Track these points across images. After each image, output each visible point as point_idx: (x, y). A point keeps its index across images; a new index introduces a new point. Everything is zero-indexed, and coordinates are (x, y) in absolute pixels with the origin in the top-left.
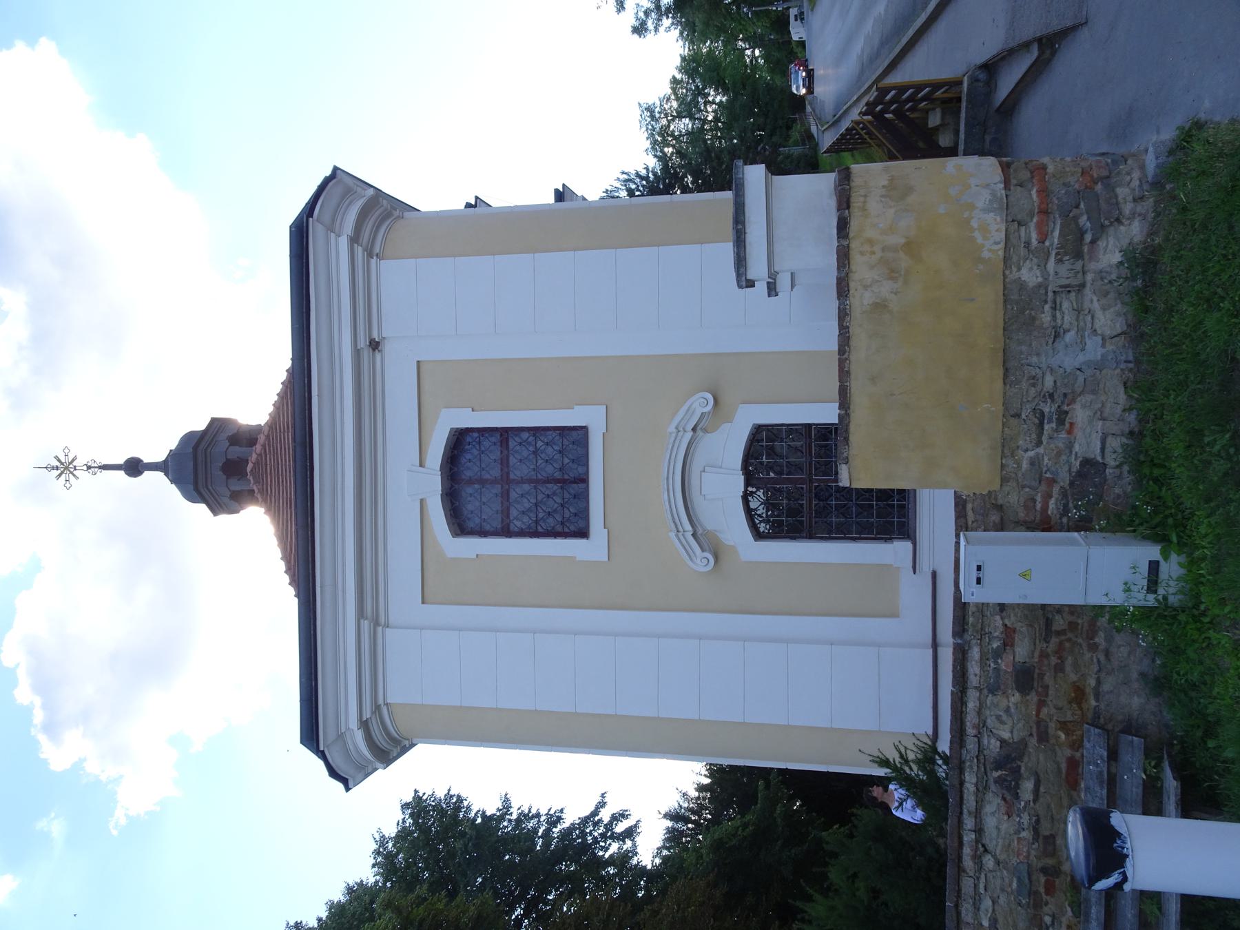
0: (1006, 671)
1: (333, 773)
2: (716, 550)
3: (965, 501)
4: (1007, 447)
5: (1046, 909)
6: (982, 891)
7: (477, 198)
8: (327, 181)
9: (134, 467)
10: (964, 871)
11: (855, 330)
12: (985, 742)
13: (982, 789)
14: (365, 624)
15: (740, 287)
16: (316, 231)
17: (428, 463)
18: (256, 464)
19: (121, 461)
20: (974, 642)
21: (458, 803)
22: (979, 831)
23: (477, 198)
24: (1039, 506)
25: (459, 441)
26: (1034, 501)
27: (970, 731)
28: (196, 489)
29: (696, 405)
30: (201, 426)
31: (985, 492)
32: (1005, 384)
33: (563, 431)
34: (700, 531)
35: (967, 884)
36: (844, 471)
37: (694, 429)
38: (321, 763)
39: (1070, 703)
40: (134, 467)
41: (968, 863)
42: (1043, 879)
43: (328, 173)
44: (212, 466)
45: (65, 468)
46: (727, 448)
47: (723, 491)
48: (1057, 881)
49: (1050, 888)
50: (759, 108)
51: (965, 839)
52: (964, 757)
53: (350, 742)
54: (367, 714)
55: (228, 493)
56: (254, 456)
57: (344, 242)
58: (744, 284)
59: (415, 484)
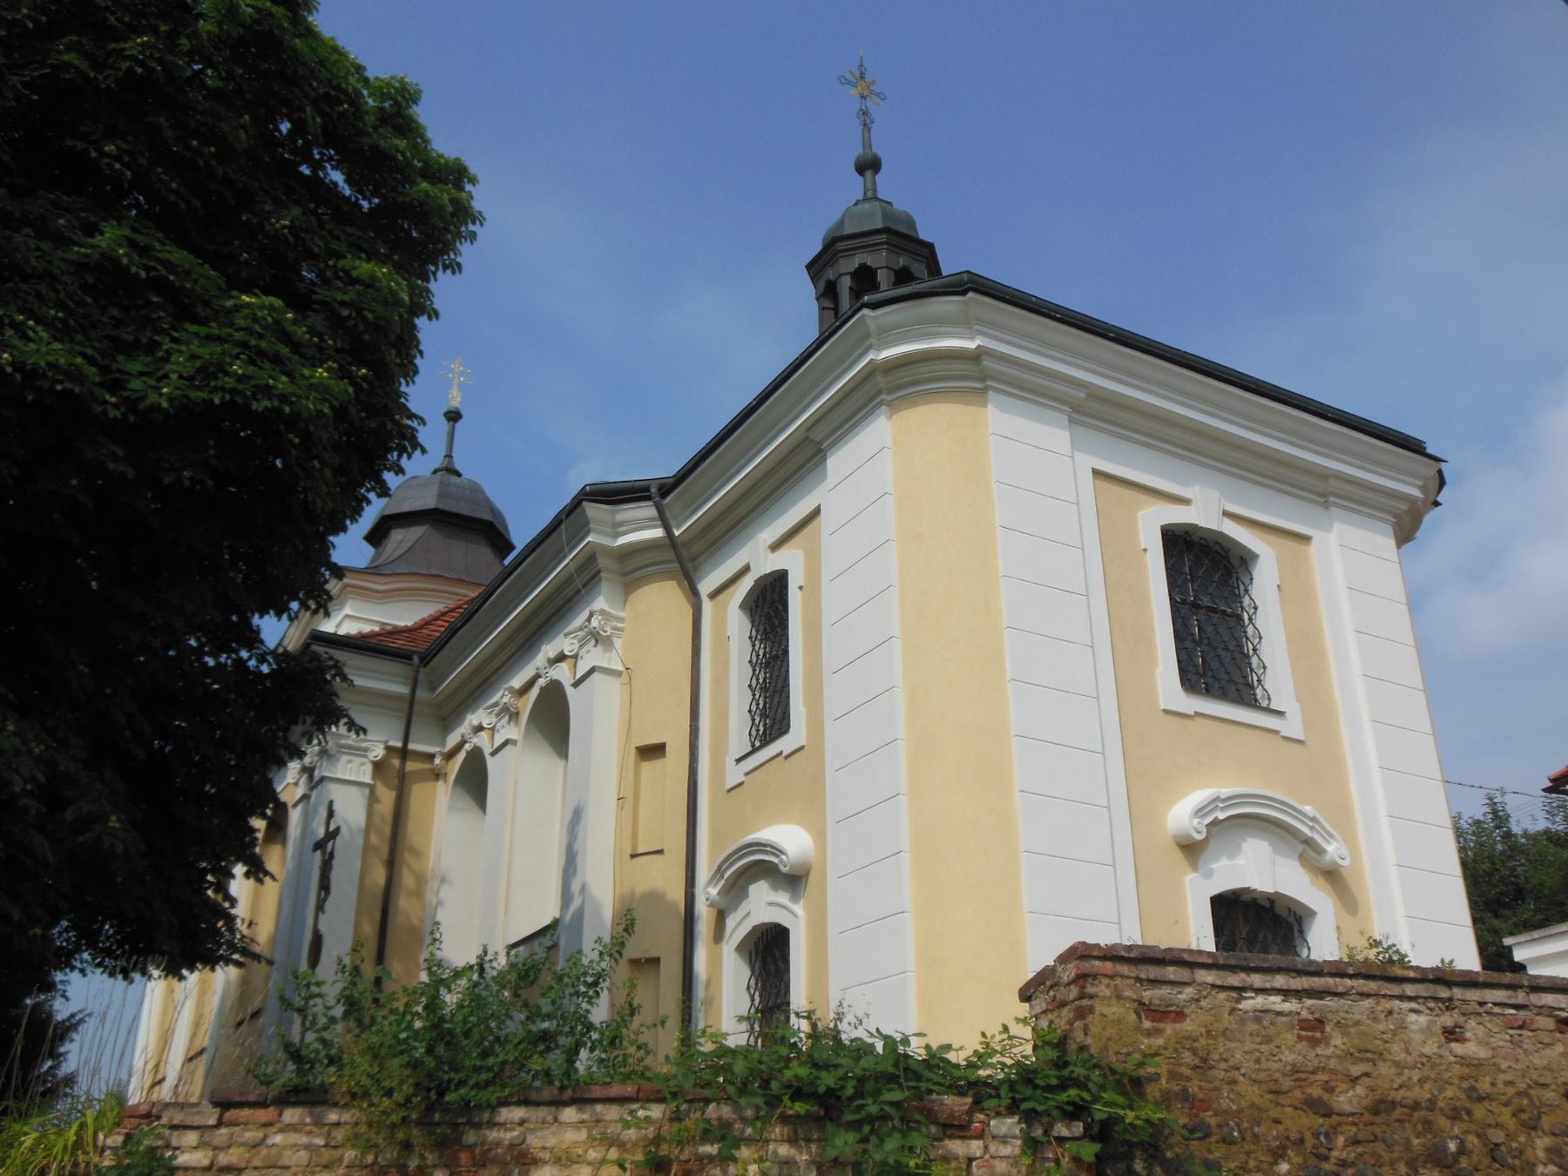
9: (868, 166)
19: (877, 149)
40: (868, 166)
54: (987, 363)
59: (1207, 506)
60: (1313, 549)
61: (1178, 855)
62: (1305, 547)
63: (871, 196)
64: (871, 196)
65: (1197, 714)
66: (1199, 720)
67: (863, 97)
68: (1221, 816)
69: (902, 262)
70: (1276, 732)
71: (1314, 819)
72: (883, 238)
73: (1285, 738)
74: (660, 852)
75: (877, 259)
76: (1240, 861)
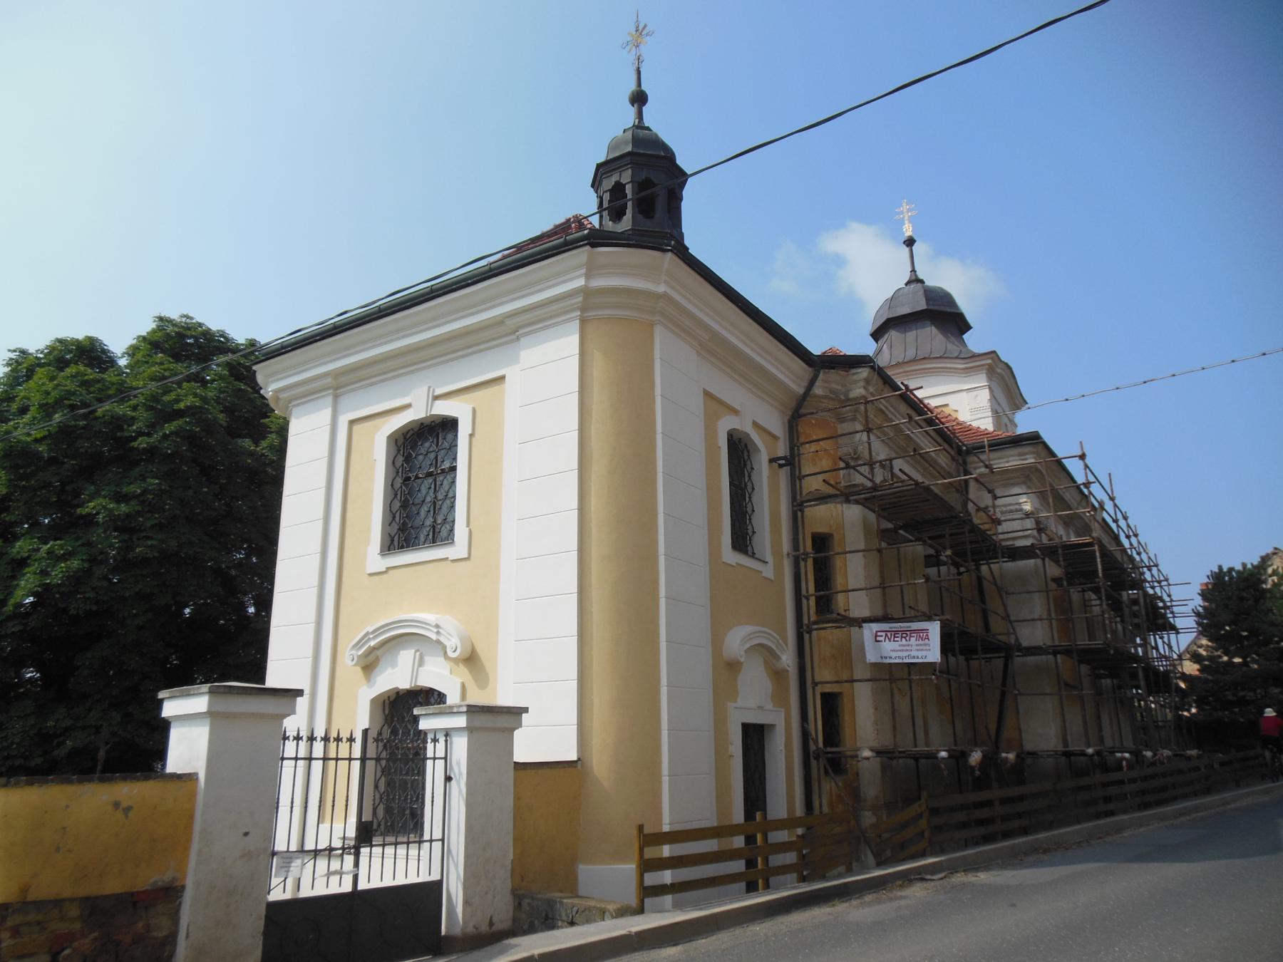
2: (369, 664)
9: (639, 99)
14: (329, 380)
34: (378, 653)
40: (639, 99)
45: (640, 31)
46: (437, 674)
47: (398, 675)
57: (580, 282)
59: (415, 402)
63: (640, 126)
64: (640, 126)
68: (372, 643)
73: (453, 561)
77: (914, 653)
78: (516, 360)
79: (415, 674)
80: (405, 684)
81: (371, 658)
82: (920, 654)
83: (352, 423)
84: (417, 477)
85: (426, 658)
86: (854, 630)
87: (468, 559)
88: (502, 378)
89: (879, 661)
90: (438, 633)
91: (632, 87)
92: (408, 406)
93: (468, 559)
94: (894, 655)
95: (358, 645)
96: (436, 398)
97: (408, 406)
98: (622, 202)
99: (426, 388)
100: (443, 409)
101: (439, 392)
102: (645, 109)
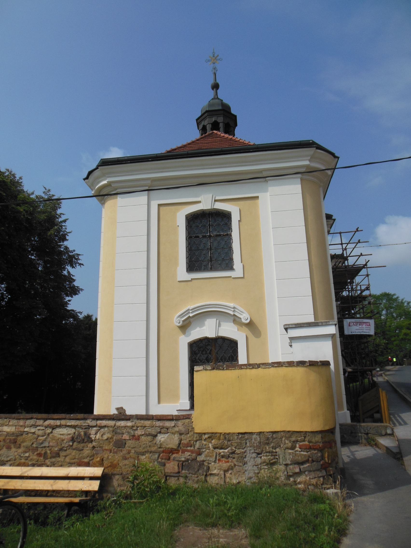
0: (122, 437)
1: (90, 173)
2: (184, 327)
3: (189, 418)
4: (212, 436)
5: (31, 454)
6: (38, 428)
7: (334, 220)
8: (333, 154)
10: (45, 421)
11: (260, 371)
12: (95, 429)
13: (74, 427)
15: (284, 326)
16: (311, 151)
17: (217, 203)
18: (217, 134)
19: (218, 81)
20: (134, 423)
21: (19, 184)
22: (60, 426)
23: (334, 220)
24: (189, 448)
25: (225, 217)
26: (191, 447)
27: (99, 422)
28: (207, 112)
29: (244, 315)
30: (233, 112)
31: (193, 426)
32: (238, 433)
33: (231, 259)
34: (191, 320)
35: (40, 422)
36: (201, 368)
37: (234, 315)
38: (94, 167)
39: (111, 462)
40: (216, 87)
41: (48, 422)
42: (43, 452)
43: (336, 155)
44: (361, 254)
46: (228, 330)
48: (42, 458)
49: (39, 455)
50: (392, 358)
51: (58, 421)
52: (88, 420)
53: (102, 179)
55: (205, 124)
56: (219, 133)
57: (307, 163)
58: (286, 327)
59: (205, 200)
60: (260, 201)
61: (178, 330)
62: (257, 201)
63: (216, 97)
64: (216, 97)
65: (192, 279)
66: (193, 281)
67: (214, 63)
68: (191, 315)
69: (214, 119)
70: (231, 277)
71: (234, 308)
72: (206, 114)
73: (233, 278)
74: (371, 255)
75: (220, 119)
76: (204, 328)
77: (364, 331)
78: (266, 191)
79: (217, 331)
80: (211, 335)
81: (187, 322)
82: (367, 331)
83: (159, 205)
84: (204, 237)
85: (221, 323)
86: (336, 321)
87: (243, 278)
88: (257, 197)
89: (350, 334)
90: (234, 311)
91: (212, 82)
92: (200, 202)
93: (243, 278)
94: (357, 331)
95: (181, 316)
96: (215, 201)
97: (200, 202)
98: (221, 129)
99: (211, 195)
100: (220, 206)
101: (217, 198)
102: (218, 91)
